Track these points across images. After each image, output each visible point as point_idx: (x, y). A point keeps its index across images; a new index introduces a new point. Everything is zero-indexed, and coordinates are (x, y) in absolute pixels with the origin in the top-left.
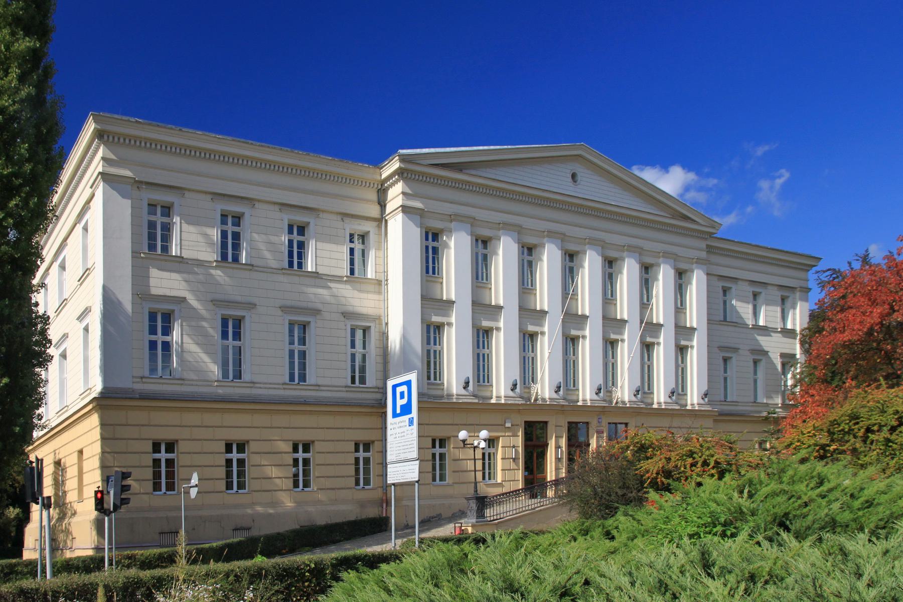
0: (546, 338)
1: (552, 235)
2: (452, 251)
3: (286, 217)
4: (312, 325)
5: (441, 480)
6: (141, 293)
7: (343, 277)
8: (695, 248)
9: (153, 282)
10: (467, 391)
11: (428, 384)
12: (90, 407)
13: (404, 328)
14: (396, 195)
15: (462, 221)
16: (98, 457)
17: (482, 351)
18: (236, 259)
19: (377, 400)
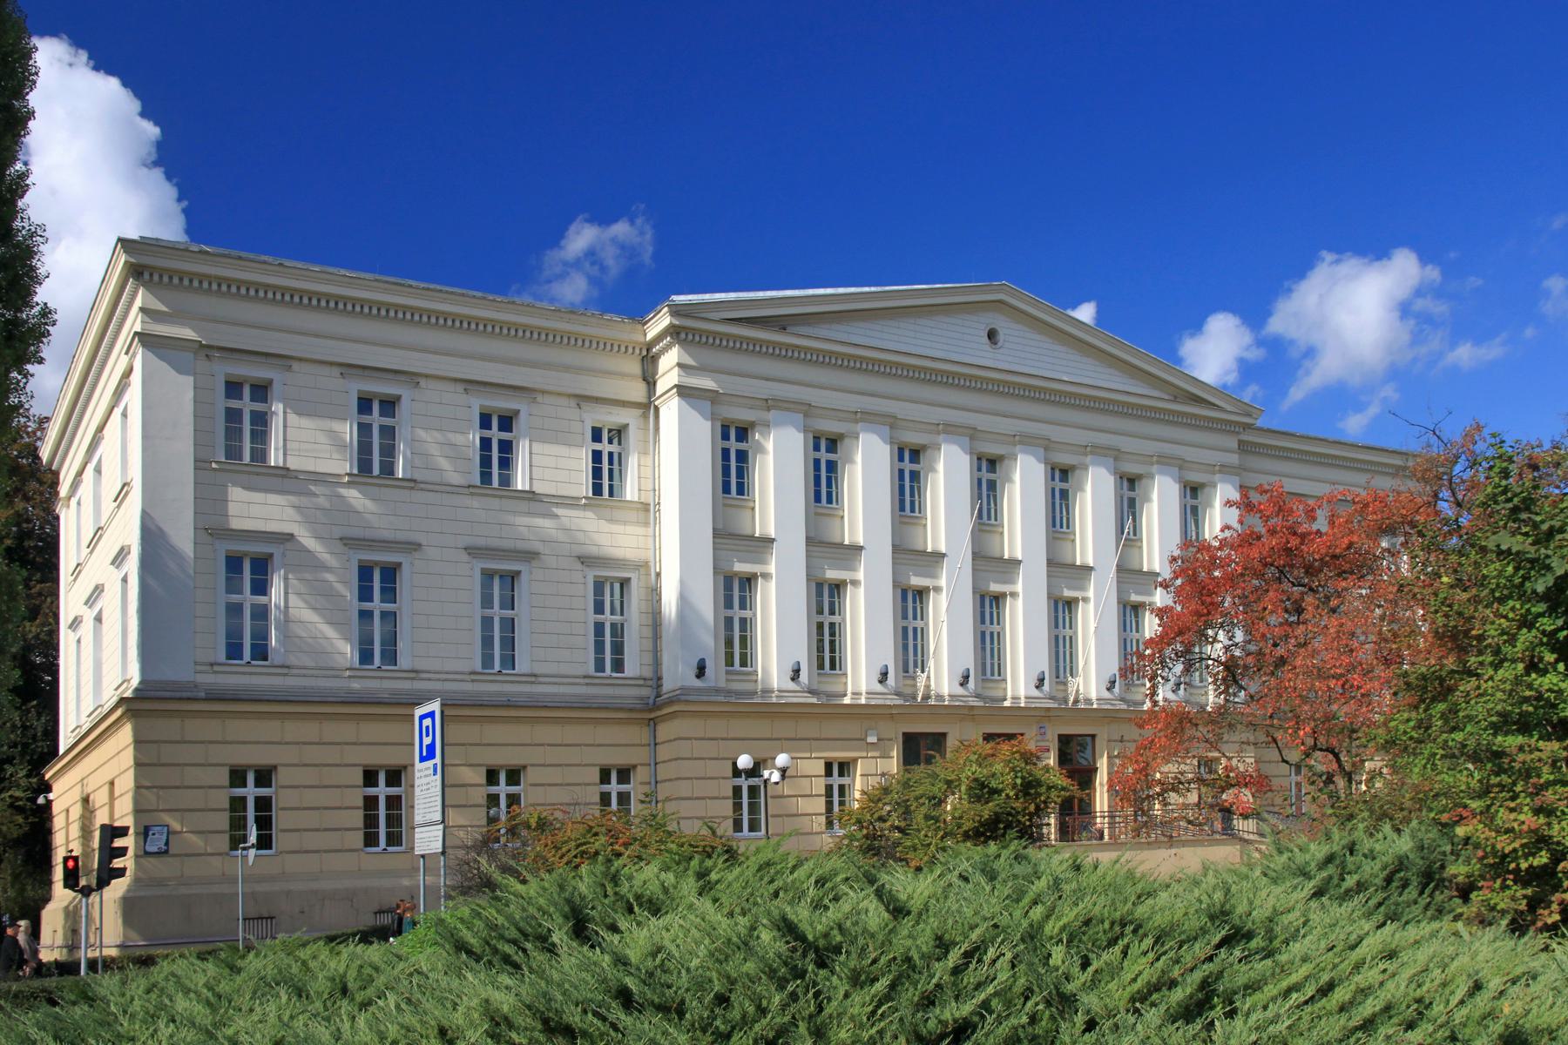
0: (1091, 605)
1: (1165, 461)
2: (770, 458)
3: (477, 403)
4: (524, 577)
5: (751, 829)
6: (212, 528)
7: (579, 499)
8: (1222, 448)
9: (233, 509)
10: (799, 683)
11: (727, 673)
12: (119, 712)
13: (682, 582)
14: (670, 363)
15: (787, 409)
16: (130, 795)
17: (988, 628)
18: (388, 469)
19: (641, 698)
